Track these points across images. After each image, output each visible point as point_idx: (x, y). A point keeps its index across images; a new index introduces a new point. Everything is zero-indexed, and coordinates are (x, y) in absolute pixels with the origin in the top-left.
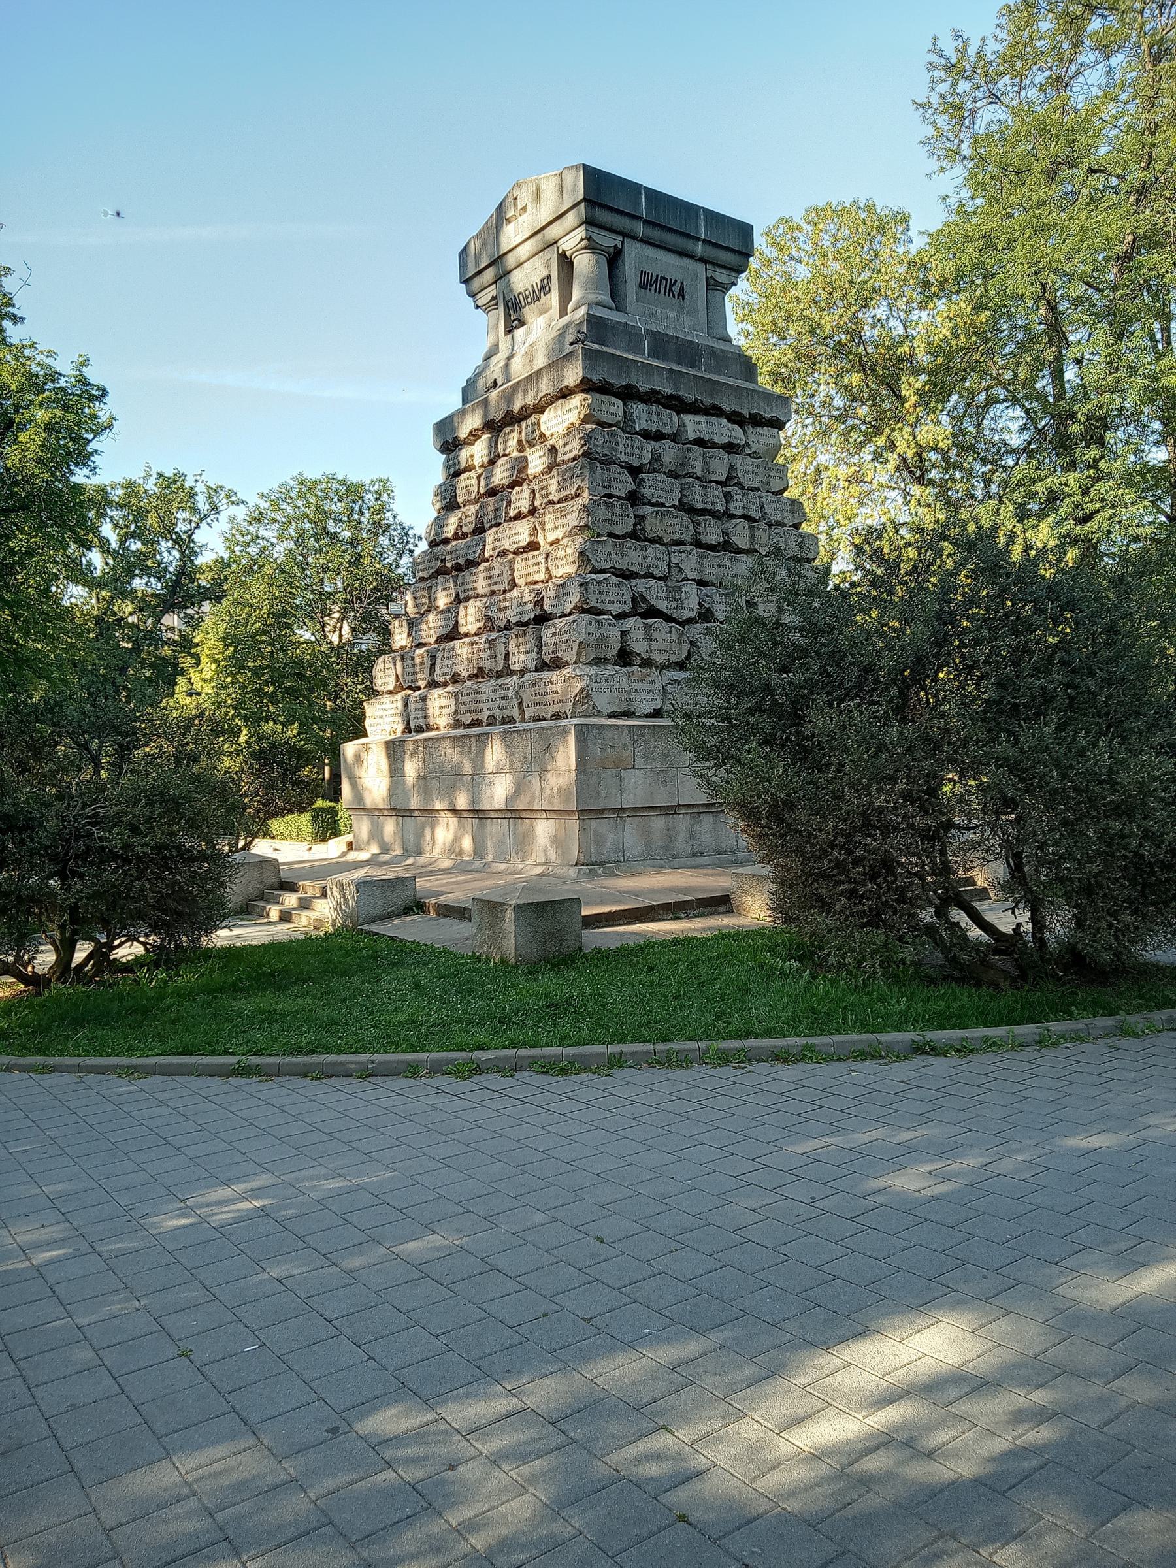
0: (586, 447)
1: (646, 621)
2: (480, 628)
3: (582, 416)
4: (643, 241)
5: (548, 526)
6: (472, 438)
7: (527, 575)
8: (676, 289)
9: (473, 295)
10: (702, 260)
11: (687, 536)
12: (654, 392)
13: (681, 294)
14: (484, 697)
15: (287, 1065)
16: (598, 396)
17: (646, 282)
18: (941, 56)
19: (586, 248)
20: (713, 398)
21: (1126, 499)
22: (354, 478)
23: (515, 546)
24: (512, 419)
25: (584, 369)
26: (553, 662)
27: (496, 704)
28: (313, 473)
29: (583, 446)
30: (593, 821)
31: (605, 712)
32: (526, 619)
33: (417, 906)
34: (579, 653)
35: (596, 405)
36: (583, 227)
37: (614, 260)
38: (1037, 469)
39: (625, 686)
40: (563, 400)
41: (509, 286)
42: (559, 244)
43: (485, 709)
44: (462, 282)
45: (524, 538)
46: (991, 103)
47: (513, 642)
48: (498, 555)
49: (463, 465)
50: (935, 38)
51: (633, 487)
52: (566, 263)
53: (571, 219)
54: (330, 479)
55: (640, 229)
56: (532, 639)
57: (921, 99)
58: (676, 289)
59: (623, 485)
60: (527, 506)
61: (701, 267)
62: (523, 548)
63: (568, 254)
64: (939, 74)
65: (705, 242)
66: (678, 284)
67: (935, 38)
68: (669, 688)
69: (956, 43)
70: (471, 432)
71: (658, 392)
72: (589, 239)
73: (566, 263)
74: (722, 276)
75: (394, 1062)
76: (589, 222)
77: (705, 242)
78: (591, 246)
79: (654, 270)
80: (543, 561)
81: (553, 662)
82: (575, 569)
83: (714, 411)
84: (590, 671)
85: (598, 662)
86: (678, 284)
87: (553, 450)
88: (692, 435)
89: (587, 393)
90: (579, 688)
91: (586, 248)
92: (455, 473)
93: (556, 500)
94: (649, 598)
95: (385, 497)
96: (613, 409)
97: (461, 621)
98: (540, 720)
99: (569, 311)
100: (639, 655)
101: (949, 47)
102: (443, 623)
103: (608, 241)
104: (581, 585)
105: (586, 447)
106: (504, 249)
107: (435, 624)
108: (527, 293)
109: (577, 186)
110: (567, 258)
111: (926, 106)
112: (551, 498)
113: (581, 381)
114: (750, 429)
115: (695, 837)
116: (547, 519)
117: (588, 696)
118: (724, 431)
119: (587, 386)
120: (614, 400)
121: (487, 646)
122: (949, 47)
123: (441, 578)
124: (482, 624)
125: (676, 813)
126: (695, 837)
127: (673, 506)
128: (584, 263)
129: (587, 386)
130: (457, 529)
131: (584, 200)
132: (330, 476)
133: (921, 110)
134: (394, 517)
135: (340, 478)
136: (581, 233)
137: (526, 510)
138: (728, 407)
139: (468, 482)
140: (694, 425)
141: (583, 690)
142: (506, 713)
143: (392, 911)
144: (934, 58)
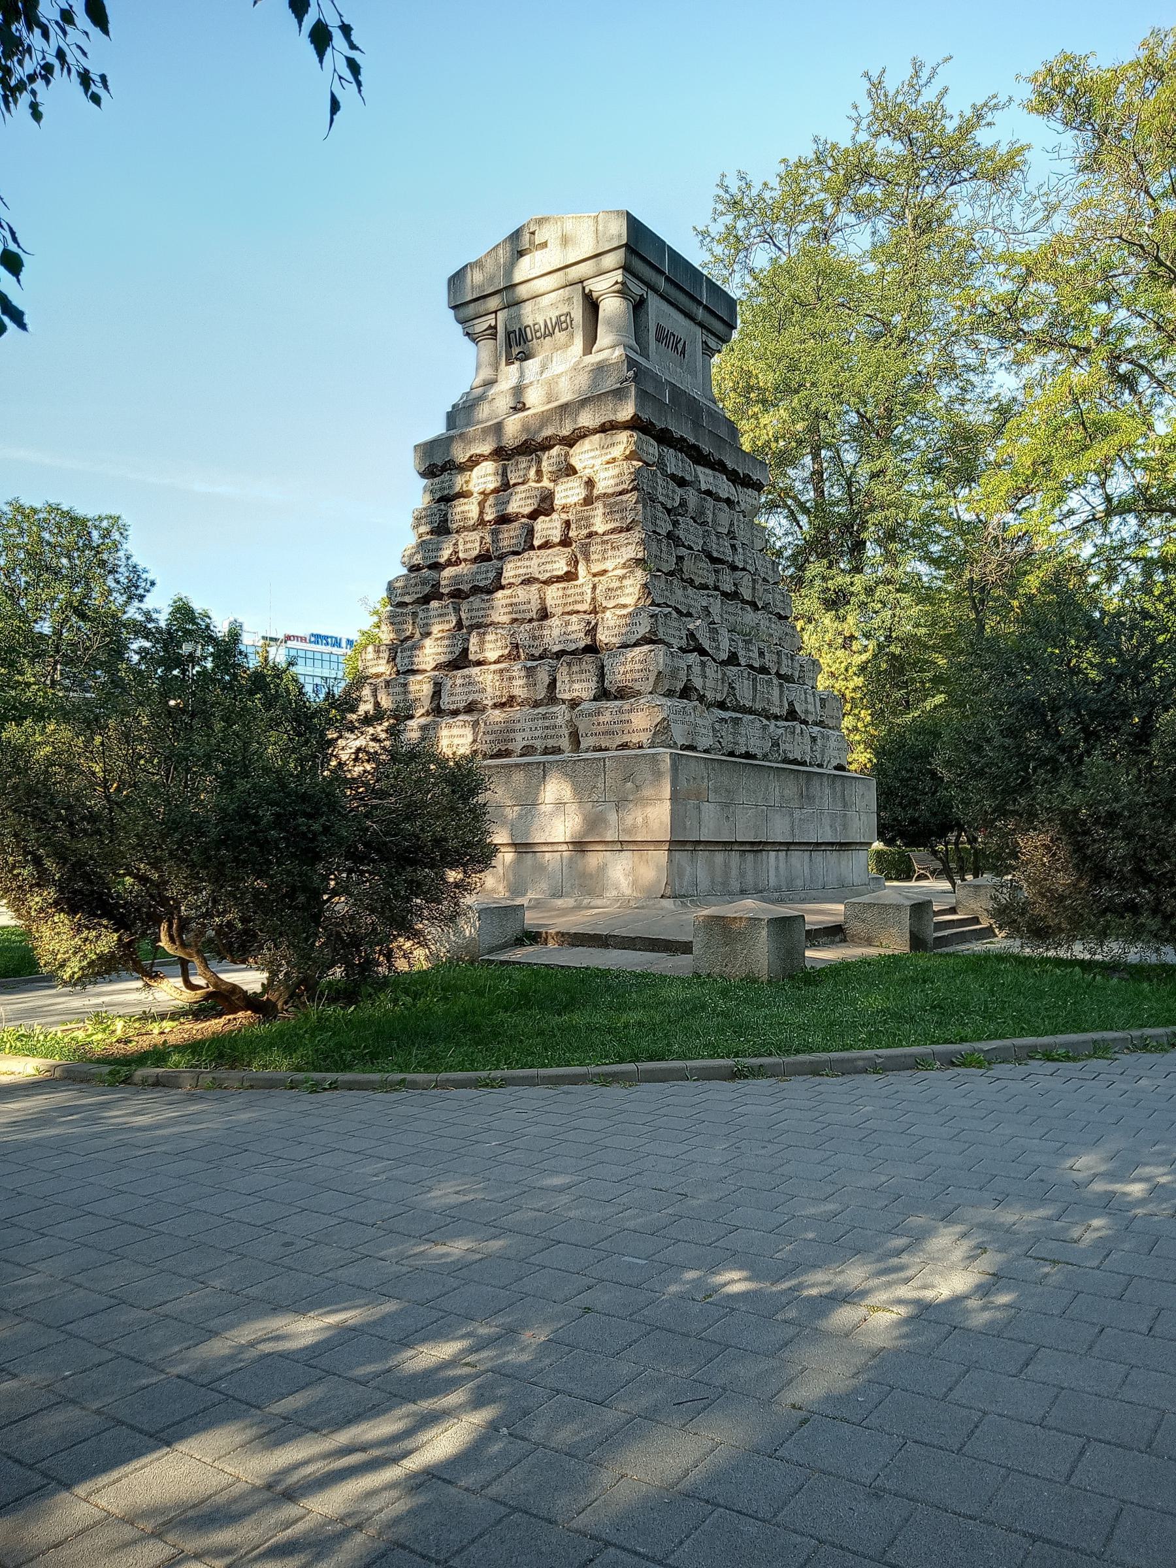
0: (636, 483)
1: (702, 658)
2: (502, 656)
3: (627, 452)
4: (662, 296)
5: (593, 557)
6: (469, 464)
7: (565, 605)
8: (680, 347)
9: (462, 321)
10: (701, 325)
11: (711, 583)
12: (683, 439)
13: (683, 352)
14: (518, 726)
15: (793, 1064)
16: (643, 437)
17: (663, 336)
18: (726, 191)
19: (618, 292)
20: (720, 454)
21: (903, 603)
22: (81, 511)
23: (548, 575)
24: (531, 448)
25: (636, 405)
26: (618, 692)
27: (537, 733)
28: (33, 500)
29: (633, 481)
30: (677, 853)
31: (679, 744)
32: (574, 648)
33: (533, 937)
34: (656, 684)
35: (639, 443)
36: (620, 271)
37: (638, 307)
38: (828, 568)
39: (692, 720)
40: (603, 435)
41: (519, 316)
42: (585, 283)
43: (519, 739)
44: (451, 308)
45: (561, 567)
46: (764, 241)
47: (564, 670)
48: (522, 583)
49: (457, 489)
50: (723, 175)
51: (670, 528)
52: (592, 305)
53: (611, 261)
54: (53, 509)
55: (662, 284)
56: (592, 668)
57: (701, 228)
58: (680, 347)
59: (665, 527)
60: (559, 535)
61: (698, 330)
62: (558, 577)
63: (595, 295)
64: (721, 207)
65: (706, 308)
66: (682, 342)
67: (723, 175)
68: (717, 726)
69: (740, 183)
70: (471, 457)
71: (685, 440)
72: (623, 283)
73: (592, 305)
74: (712, 343)
75: (901, 1056)
76: (626, 268)
77: (706, 308)
78: (623, 291)
79: (668, 325)
80: (589, 591)
81: (618, 692)
82: (634, 601)
83: (719, 467)
84: (668, 702)
85: (669, 694)
86: (682, 342)
87: (590, 483)
88: (704, 487)
89: (632, 430)
90: (661, 717)
91: (618, 292)
92: (446, 499)
93: (600, 531)
94: (698, 636)
95: (116, 536)
96: (651, 450)
97: (472, 649)
98: (601, 750)
99: (593, 351)
100: (696, 690)
101: (734, 185)
102: (445, 650)
103: (637, 289)
104: (652, 616)
105: (636, 483)
106: (517, 280)
107: (433, 651)
108: (537, 327)
109: (617, 230)
110: (592, 299)
111: (705, 234)
112: (594, 529)
113: (632, 418)
114: (740, 488)
115: (742, 874)
116: (592, 549)
117: (668, 727)
118: (725, 488)
119: (635, 425)
120: (652, 441)
121: (523, 673)
122: (734, 185)
123: (434, 604)
124: (506, 651)
125: (731, 850)
126: (742, 874)
127: (698, 551)
128: (612, 306)
129: (635, 425)
130: (451, 555)
131: (626, 245)
132: (54, 506)
133: (700, 237)
134: (128, 558)
135: (65, 509)
136: (618, 276)
137: (557, 540)
138: (730, 465)
139: (466, 508)
140: (706, 477)
141: (664, 719)
142: (551, 743)
143: (506, 942)
144: (721, 192)
